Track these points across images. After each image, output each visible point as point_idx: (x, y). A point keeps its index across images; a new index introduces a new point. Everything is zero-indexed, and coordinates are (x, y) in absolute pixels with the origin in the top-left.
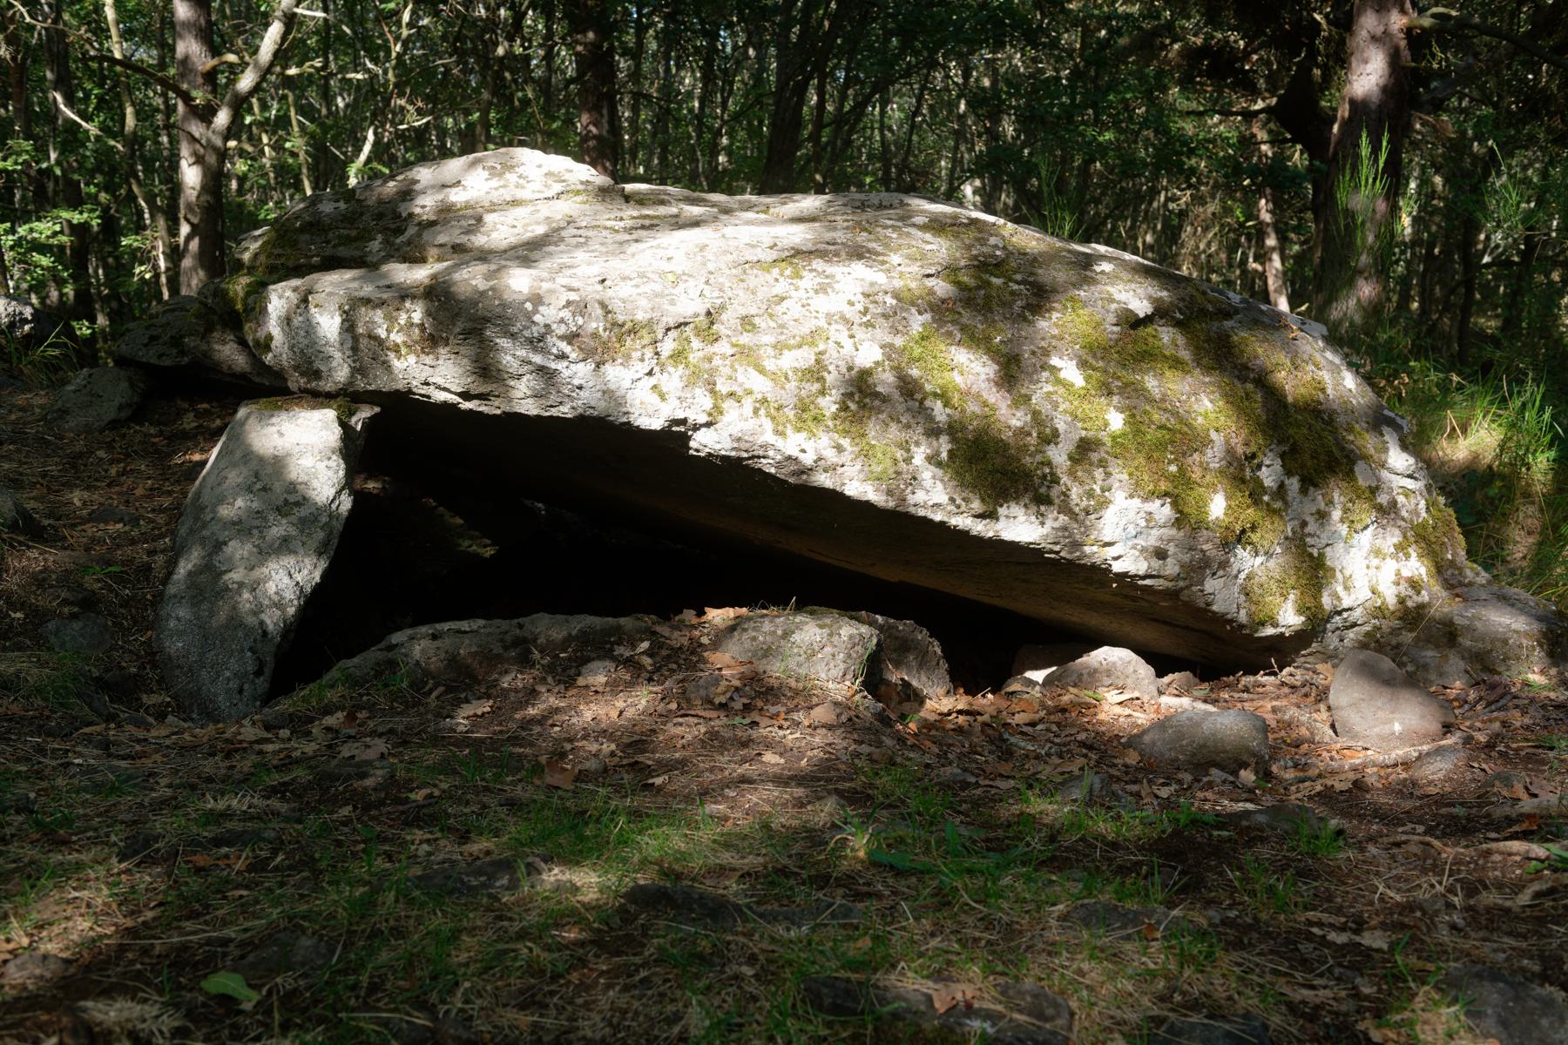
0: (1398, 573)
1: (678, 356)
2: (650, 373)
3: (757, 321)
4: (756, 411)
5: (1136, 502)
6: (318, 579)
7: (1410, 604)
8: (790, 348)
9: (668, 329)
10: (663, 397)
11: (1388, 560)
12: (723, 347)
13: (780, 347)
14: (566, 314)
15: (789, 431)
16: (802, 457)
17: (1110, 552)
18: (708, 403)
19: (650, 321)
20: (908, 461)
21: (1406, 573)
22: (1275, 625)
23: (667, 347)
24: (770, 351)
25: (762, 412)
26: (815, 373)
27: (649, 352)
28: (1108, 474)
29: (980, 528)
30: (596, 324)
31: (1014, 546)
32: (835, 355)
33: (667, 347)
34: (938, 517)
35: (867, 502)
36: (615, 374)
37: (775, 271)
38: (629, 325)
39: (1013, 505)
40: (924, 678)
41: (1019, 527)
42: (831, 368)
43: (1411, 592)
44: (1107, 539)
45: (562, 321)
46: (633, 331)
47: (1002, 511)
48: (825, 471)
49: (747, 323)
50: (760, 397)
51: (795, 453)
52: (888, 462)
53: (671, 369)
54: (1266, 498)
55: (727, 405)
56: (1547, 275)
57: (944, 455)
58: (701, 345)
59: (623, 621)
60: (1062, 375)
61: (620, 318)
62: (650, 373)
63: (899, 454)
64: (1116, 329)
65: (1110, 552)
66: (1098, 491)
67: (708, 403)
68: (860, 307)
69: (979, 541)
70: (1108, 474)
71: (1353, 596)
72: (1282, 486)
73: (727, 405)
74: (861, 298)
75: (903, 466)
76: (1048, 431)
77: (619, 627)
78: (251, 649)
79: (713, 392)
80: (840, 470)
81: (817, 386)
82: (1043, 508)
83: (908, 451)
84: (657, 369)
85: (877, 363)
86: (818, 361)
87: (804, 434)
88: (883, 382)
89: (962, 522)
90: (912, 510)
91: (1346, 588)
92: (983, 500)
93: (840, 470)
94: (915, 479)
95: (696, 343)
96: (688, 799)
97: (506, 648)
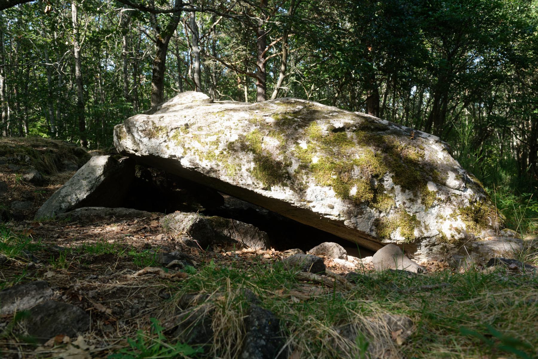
0: (451, 226)
1: (175, 137)
2: (165, 141)
3: (203, 128)
4: (194, 153)
5: (319, 188)
6: (85, 197)
7: (456, 238)
8: (210, 135)
9: (172, 129)
10: (168, 148)
11: (447, 220)
12: (190, 135)
13: (207, 135)
14: (142, 124)
15: (204, 160)
16: (206, 167)
17: (311, 205)
18: (182, 150)
19: (166, 127)
20: (240, 170)
21: (455, 226)
22: (390, 239)
23: (172, 134)
24: (204, 136)
25: (196, 154)
26: (217, 143)
27: (165, 136)
28: (308, 177)
29: (267, 194)
30: (151, 127)
31: (277, 201)
32: (224, 138)
33: (172, 134)
34: (250, 189)
35: (228, 183)
36: (154, 141)
37: (217, 115)
38: (159, 128)
39: (276, 186)
40: (252, 243)
41: (280, 193)
42: (222, 142)
43: (456, 233)
44: (308, 200)
45: (141, 126)
46: (161, 129)
47: (272, 188)
48: (213, 172)
49: (200, 128)
50: (196, 149)
51: (204, 166)
52: (233, 170)
53: (172, 141)
54: (385, 192)
55: (188, 151)
56: (480, 104)
57: (252, 169)
58: (183, 134)
59: (144, 212)
60: (300, 145)
61: (157, 126)
62: (165, 141)
63: (237, 168)
64: (327, 132)
65: (311, 205)
66: (304, 183)
67: (182, 150)
68: (236, 124)
69: (265, 198)
70: (308, 177)
71: (430, 233)
72: (393, 188)
73: (188, 151)
74: (237, 121)
75: (238, 171)
76: (288, 162)
77: (142, 213)
78: (55, 212)
79: (184, 147)
80: (218, 172)
81: (216, 147)
82: (285, 187)
83: (240, 167)
84: (167, 140)
85: (236, 140)
86: (217, 140)
87: (208, 161)
88: (236, 146)
89: (259, 191)
90: (242, 186)
91: (426, 229)
92: (264, 184)
93: (218, 172)
94: (242, 176)
95: (181, 133)
96: (420, 337)
97: (106, 215)
